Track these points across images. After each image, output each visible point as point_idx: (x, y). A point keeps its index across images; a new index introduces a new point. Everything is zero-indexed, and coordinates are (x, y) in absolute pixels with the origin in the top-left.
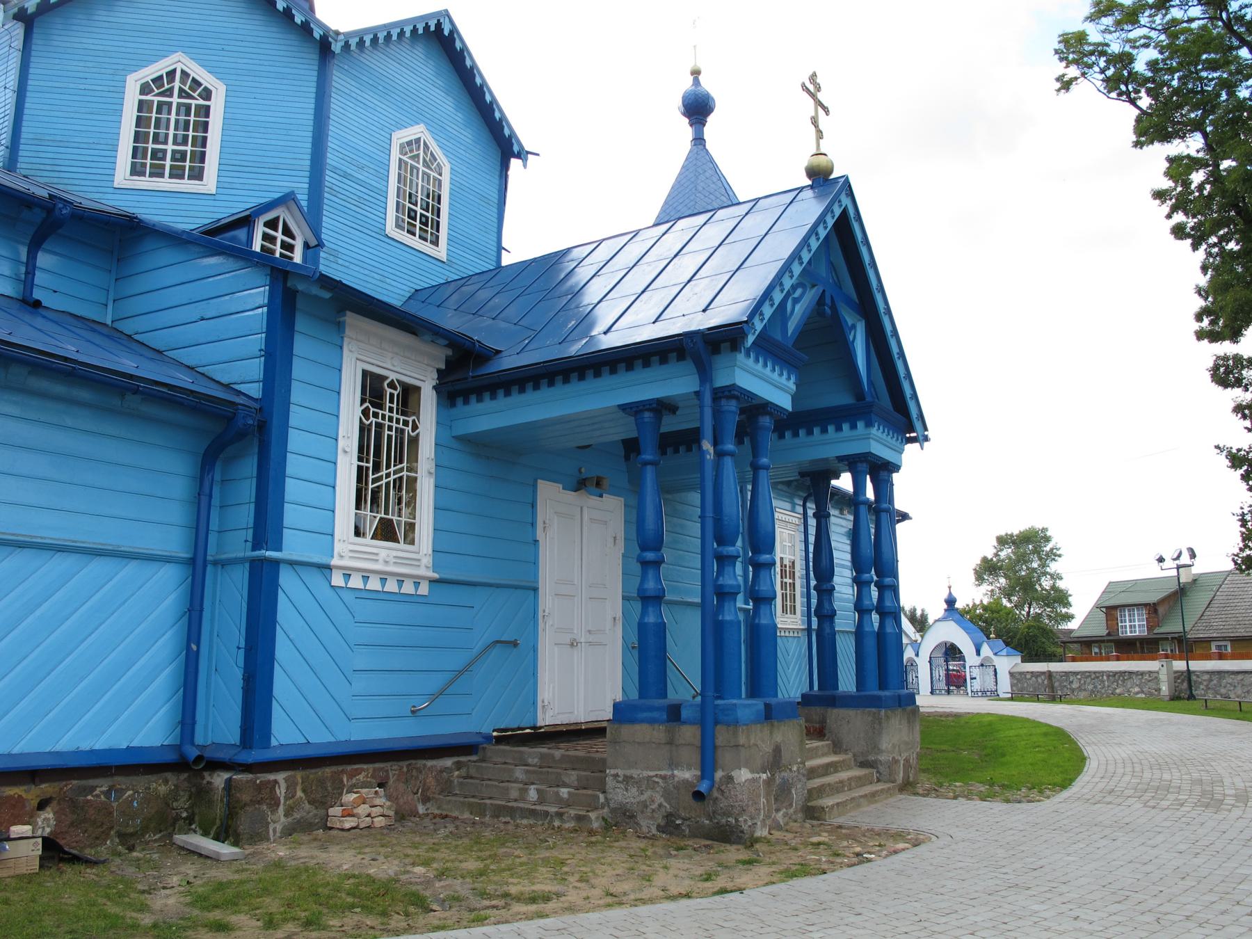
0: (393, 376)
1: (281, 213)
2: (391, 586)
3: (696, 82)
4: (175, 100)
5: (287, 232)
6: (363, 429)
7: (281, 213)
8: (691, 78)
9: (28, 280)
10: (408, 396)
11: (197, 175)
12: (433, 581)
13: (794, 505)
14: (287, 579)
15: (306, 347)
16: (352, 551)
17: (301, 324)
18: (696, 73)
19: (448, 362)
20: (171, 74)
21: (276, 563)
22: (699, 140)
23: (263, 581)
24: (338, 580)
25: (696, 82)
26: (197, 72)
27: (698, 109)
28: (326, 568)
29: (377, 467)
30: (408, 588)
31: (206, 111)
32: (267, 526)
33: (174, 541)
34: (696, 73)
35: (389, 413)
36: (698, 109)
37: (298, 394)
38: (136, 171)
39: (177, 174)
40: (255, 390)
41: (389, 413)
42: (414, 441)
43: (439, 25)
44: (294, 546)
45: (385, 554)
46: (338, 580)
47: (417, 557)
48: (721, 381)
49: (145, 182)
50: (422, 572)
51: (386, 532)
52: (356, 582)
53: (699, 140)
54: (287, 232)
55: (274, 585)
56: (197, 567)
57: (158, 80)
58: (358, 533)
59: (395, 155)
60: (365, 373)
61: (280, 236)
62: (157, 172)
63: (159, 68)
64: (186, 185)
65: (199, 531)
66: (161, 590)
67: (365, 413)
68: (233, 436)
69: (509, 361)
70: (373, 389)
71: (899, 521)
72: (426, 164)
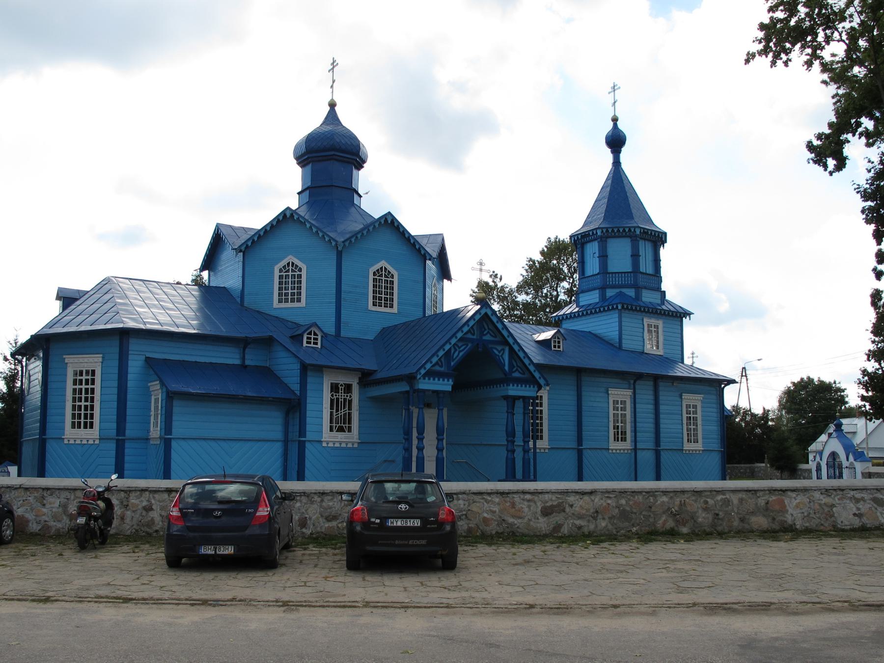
0: (341, 383)
1: (313, 329)
2: (344, 445)
3: (615, 125)
4: (383, 278)
5: (315, 334)
6: (332, 401)
7: (313, 329)
8: (612, 124)
9: (243, 359)
10: (348, 388)
11: (299, 300)
12: (359, 443)
13: (630, 384)
14: (308, 445)
15: (311, 379)
16: (330, 437)
17: (309, 373)
18: (615, 120)
19: (360, 379)
20: (288, 264)
21: (305, 441)
22: (617, 163)
23: (302, 446)
24: (324, 444)
25: (615, 125)
26: (389, 268)
27: (616, 141)
28: (321, 442)
29: (337, 411)
30: (350, 445)
31: (300, 276)
32: (302, 432)
33: (279, 435)
34: (615, 120)
35: (342, 395)
36: (616, 141)
37: (309, 393)
38: (280, 301)
39: (293, 301)
40: (298, 393)
41: (342, 395)
42: (350, 402)
43: (386, 220)
44: (310, 436)
45: (340, 436)
46: (324, 444)
47: (353, 436)
48: (416, 388)
49: (283, 305)
50: (355, 440)
51: (341, 429)
52: (331, 445)
53: (617, 163)
54: (315, 334)
55: (304, 447)
56: (286, 442)
57: (284, 267)
58: (331, 430)
59: (371, 277)
60: (332, 384)
61: (312, 336)
62: (286, 301)
63: (284, 262)
64: (388, 310)
65: (286, 432)
66: (278, 448)
67: (332, 395)
68: (293, 407)
69: (379, 376)
70: (334, 388)
71: (726, 385)
72: (386, 276)
